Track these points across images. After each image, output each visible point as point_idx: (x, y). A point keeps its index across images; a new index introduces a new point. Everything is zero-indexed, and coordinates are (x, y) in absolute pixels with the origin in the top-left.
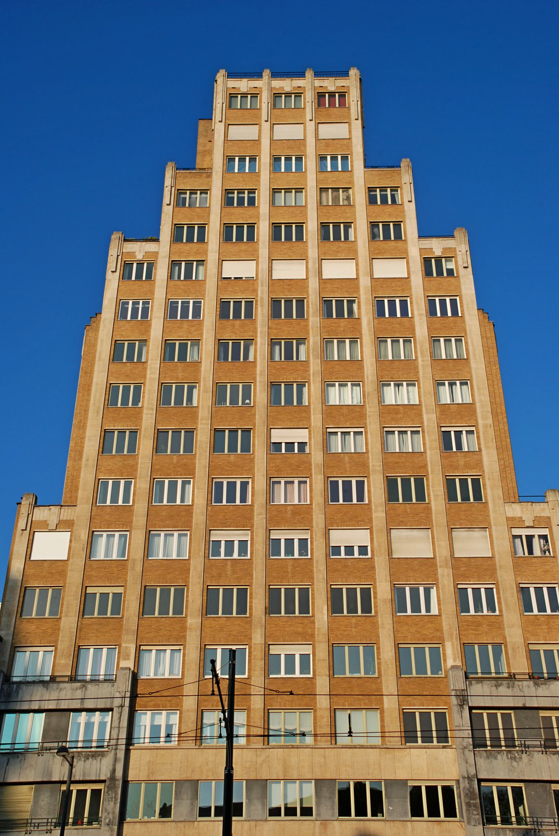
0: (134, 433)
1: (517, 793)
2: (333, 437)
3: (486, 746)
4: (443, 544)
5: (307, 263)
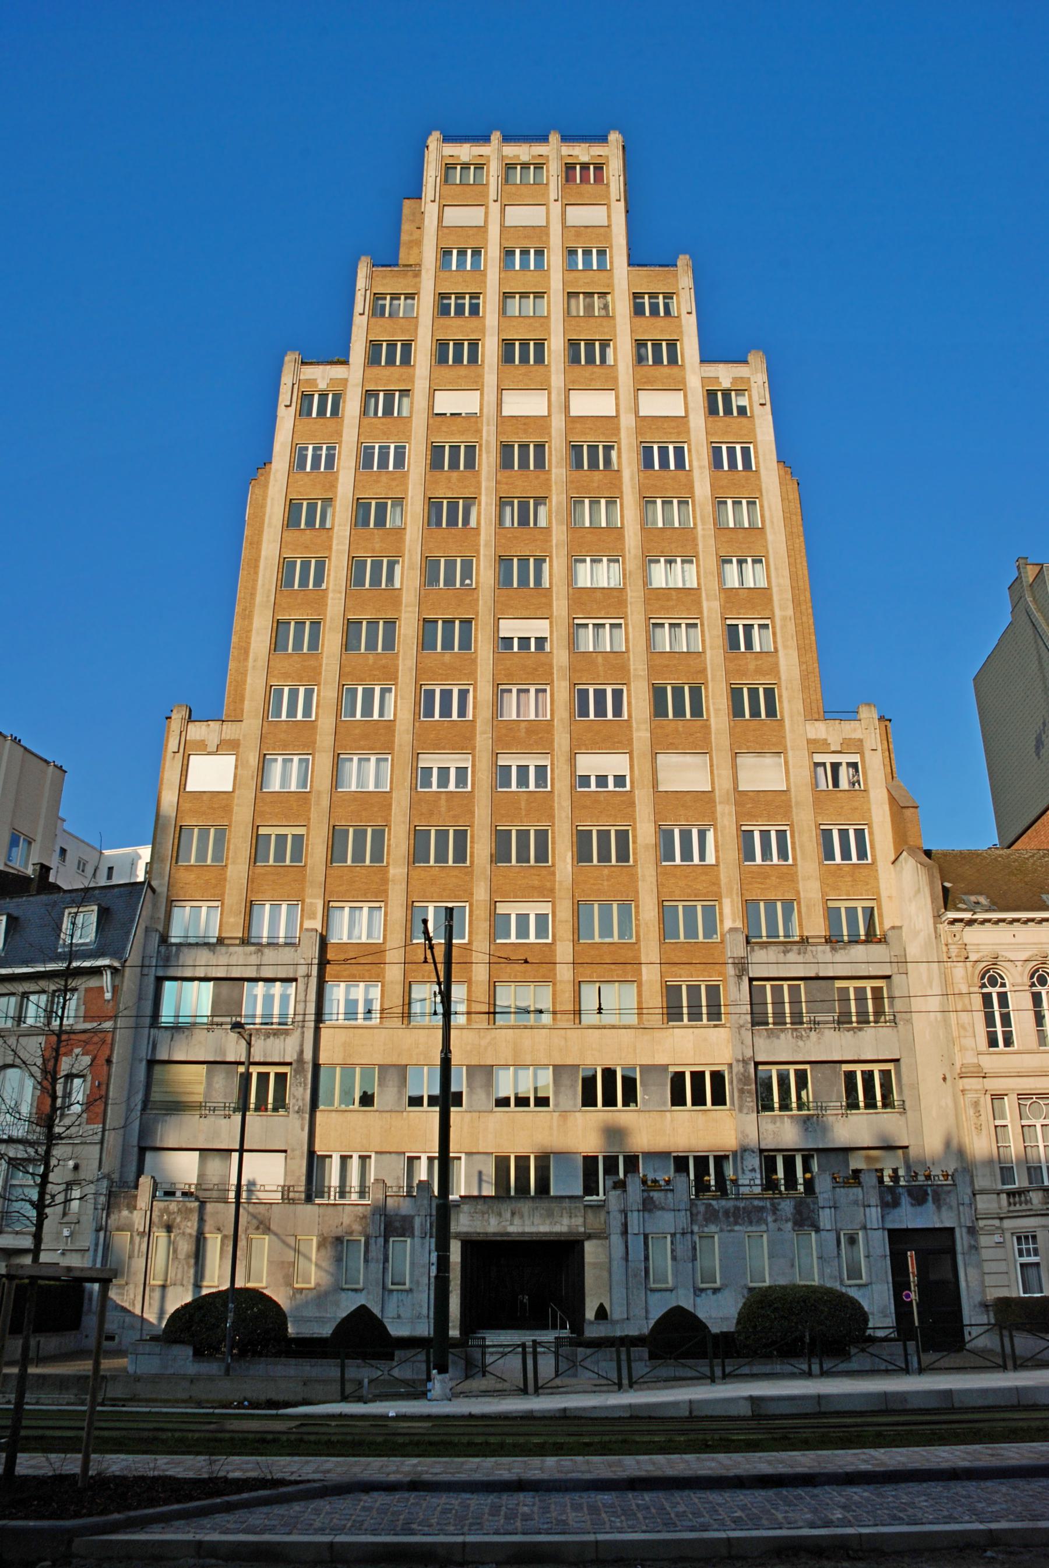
0: (316, 624)
1: (802, 1077)
2: (582, 631)
3: (767, 1024)
4: (724, 774)
5: (549, 394)
